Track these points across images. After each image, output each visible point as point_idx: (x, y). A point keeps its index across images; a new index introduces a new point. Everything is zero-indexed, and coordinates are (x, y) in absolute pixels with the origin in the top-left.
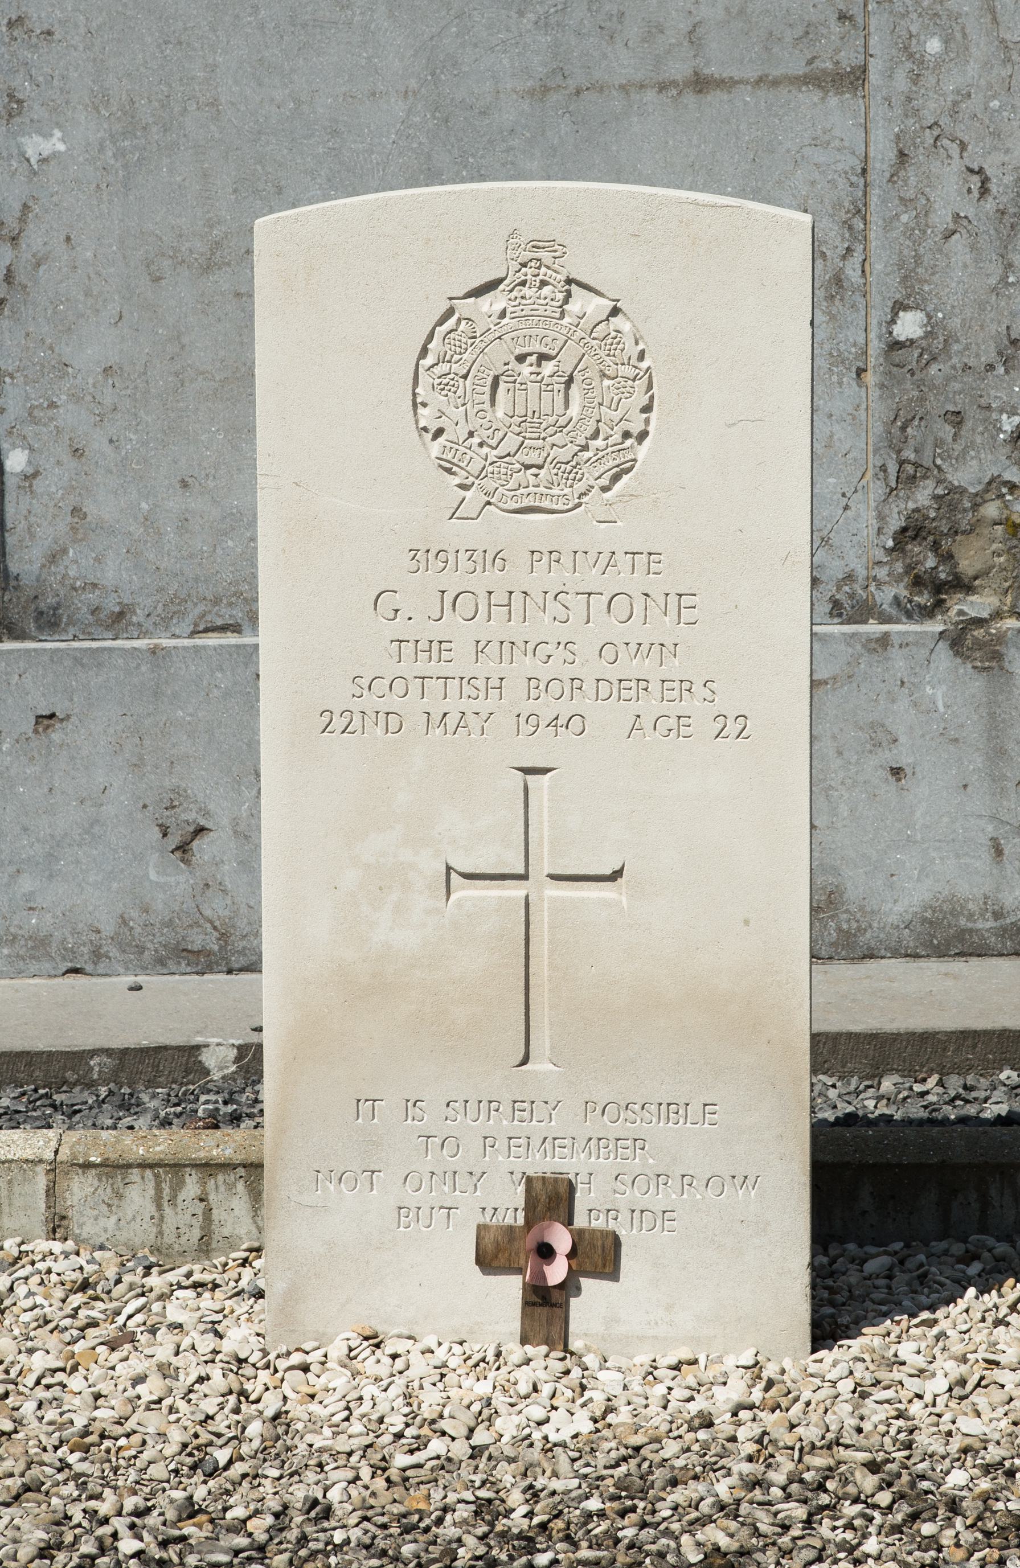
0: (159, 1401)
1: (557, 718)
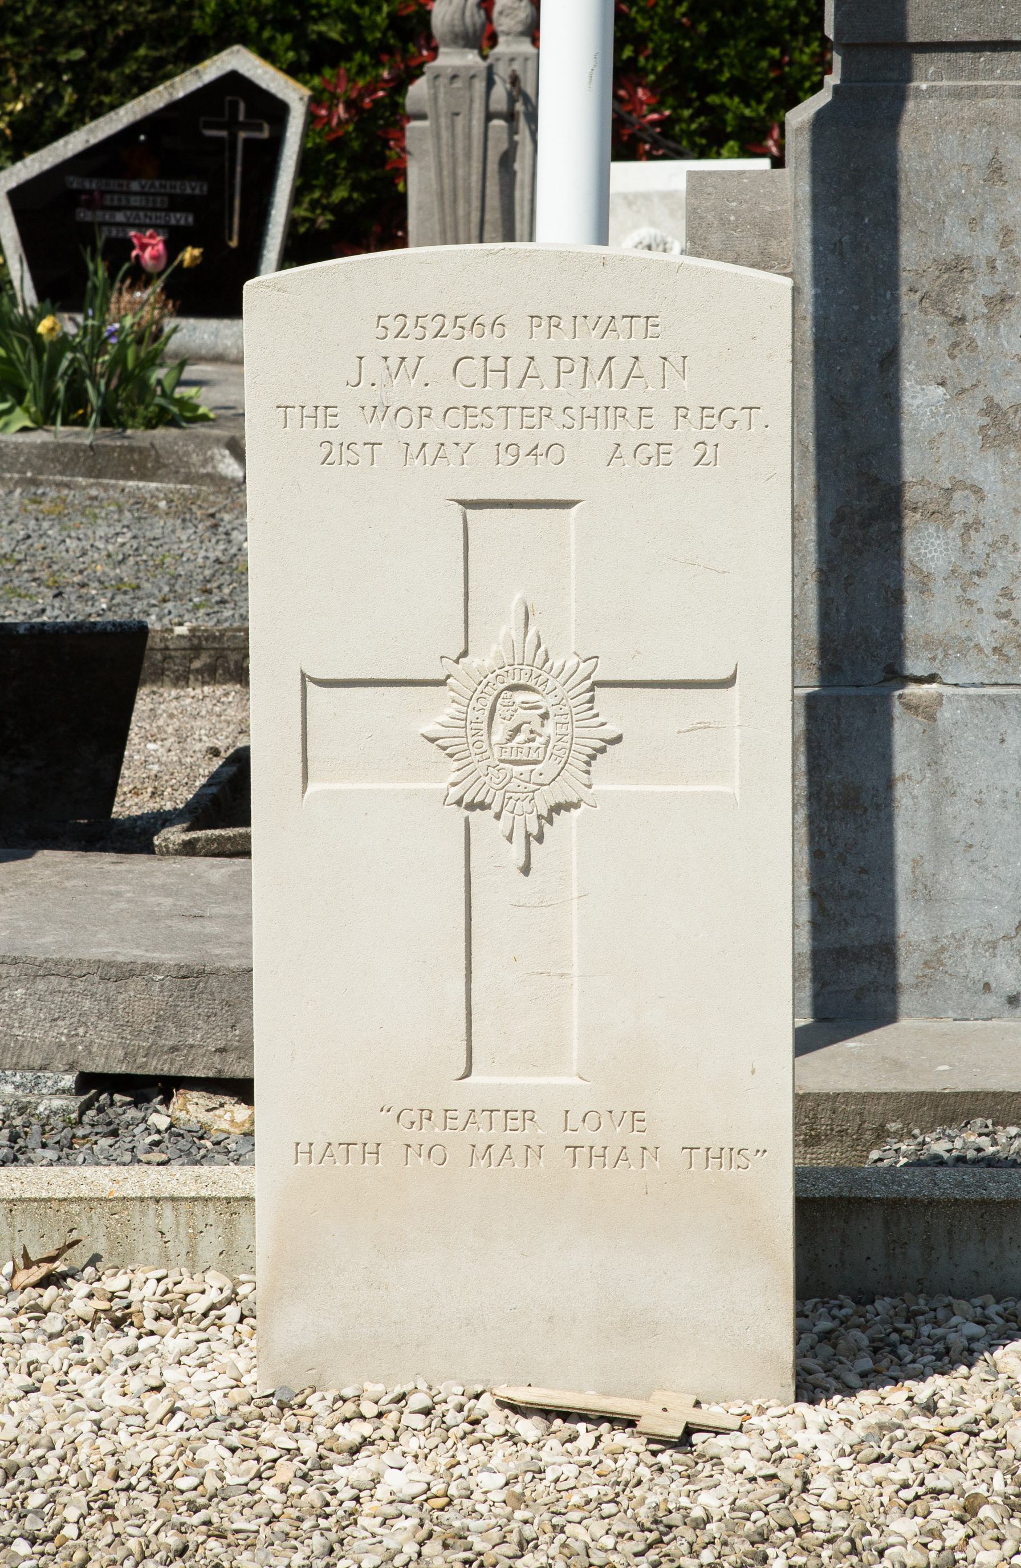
1: (536, 447)
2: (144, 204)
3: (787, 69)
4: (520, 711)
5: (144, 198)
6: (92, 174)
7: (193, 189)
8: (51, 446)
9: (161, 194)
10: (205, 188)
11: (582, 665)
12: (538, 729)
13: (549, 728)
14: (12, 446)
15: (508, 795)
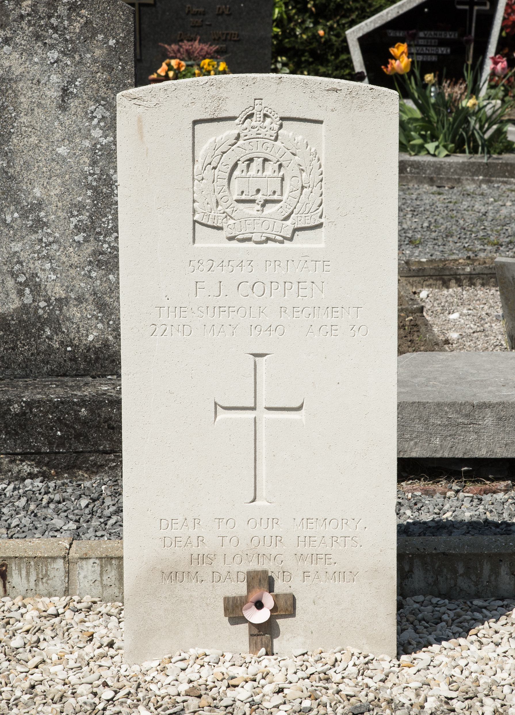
0: (72, 669)
1: (270, 326)
2: (426, 43)
5: (426, 40)
6: (400, 29)
7: (450, 35)
8: (467, 164)
9: (434, 38)
10: (456, 35)
14: (447, 164)
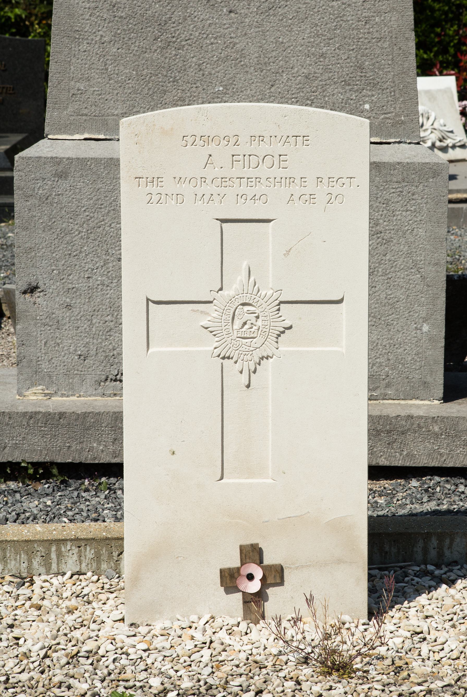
3: (443, 37)
4: (246, 314)
11: (275, 294)
12: (255, 323)
13: (259, 323)
15: (241, 352)
